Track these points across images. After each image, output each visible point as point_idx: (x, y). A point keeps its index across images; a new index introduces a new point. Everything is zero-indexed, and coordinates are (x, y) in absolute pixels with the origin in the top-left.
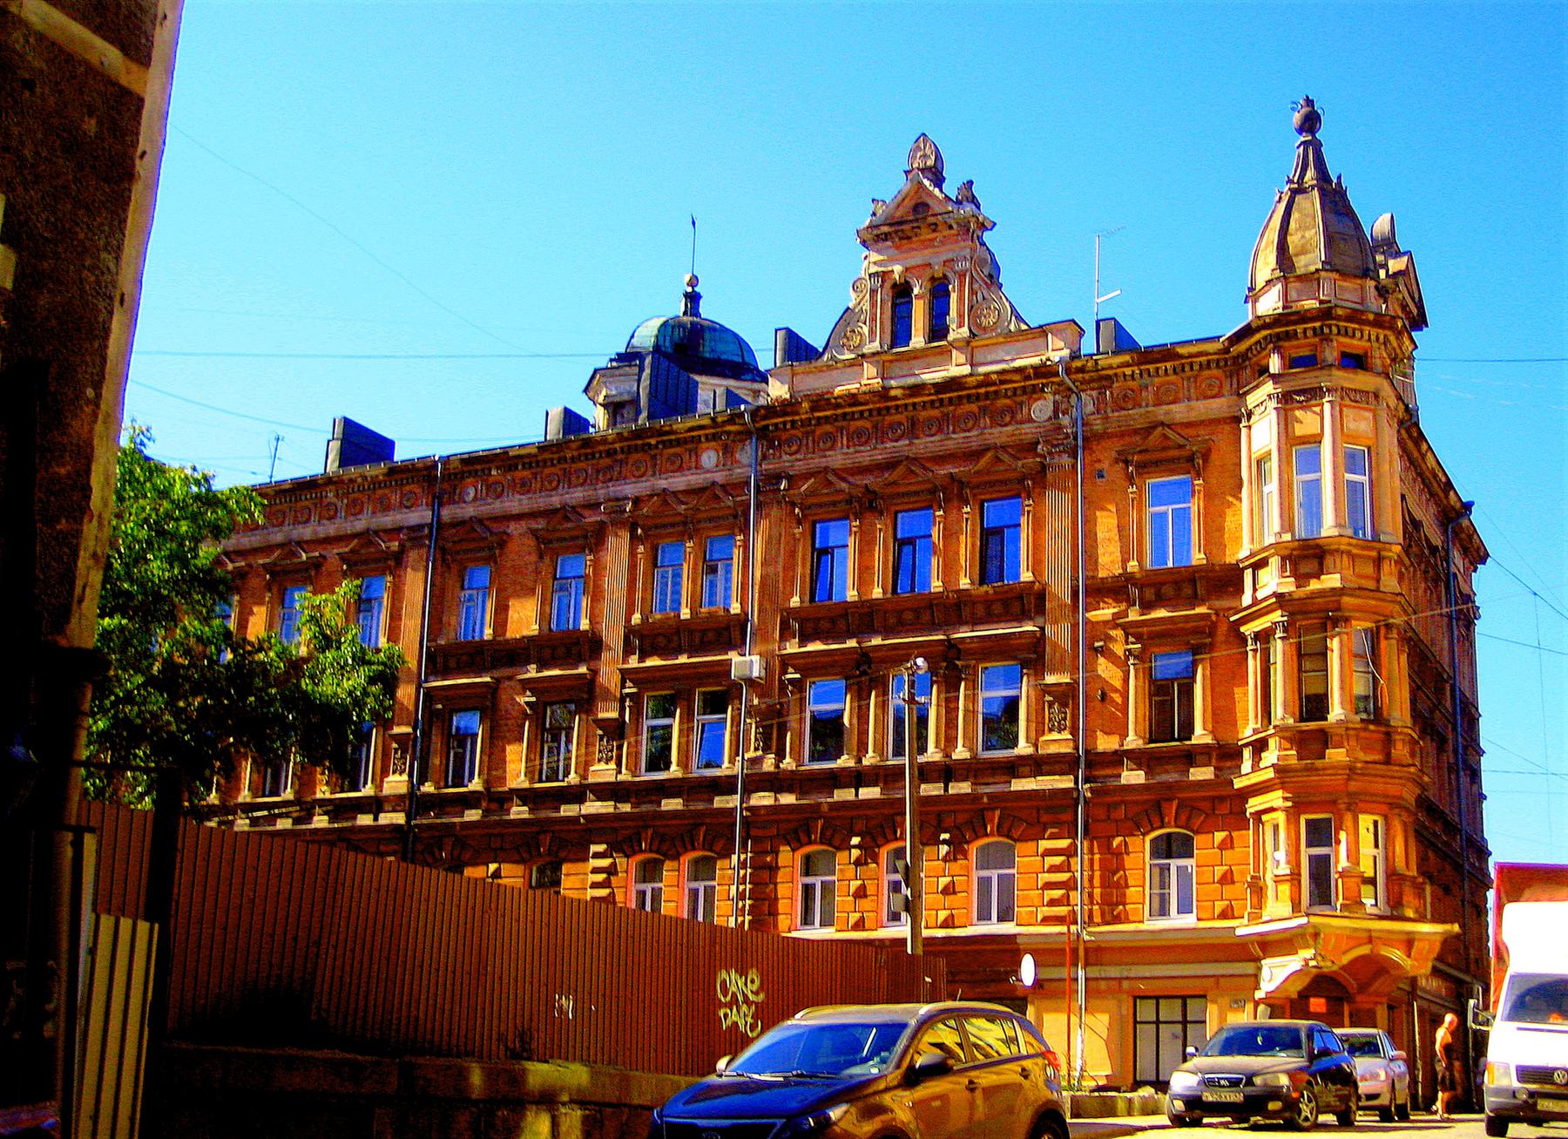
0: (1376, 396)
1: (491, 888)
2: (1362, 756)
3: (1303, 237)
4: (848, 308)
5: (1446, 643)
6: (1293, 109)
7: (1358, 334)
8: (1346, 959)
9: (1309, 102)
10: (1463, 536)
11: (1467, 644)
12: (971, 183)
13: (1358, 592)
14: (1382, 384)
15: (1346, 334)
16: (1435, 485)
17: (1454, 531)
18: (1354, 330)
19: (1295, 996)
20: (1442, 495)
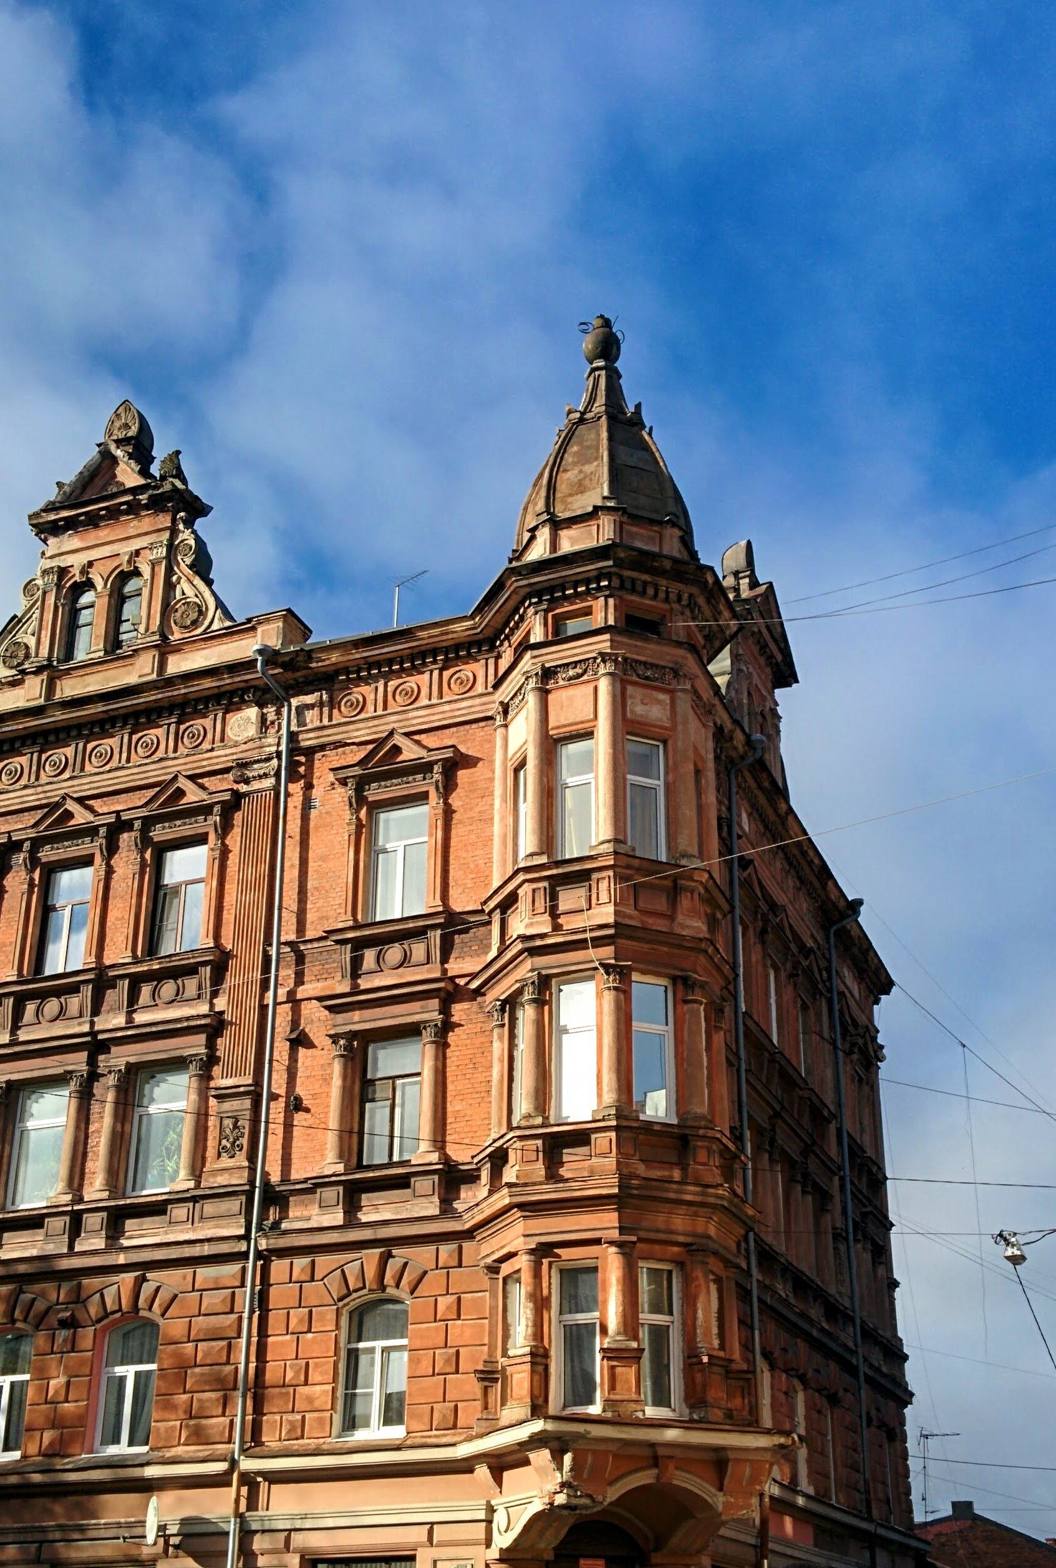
0: (676, 673)
1: (557, 1478)
2: (641, 1169)
3: (581, 471)
4: (15, 616)
5: (829, 1073)
6: (584, 332)
7: (650, 591)
8: (613, 1494)
9: (607, 323)
10: (856, 951)
11: (866, 1089)
12: (178, 453)
13: (640, 934)
14: (686, 658)
15: (633, 590)
16: (806, 868)
17: (837, 933)
18: (645, 584)
19: (549, 1556)
20: (817, 884)
